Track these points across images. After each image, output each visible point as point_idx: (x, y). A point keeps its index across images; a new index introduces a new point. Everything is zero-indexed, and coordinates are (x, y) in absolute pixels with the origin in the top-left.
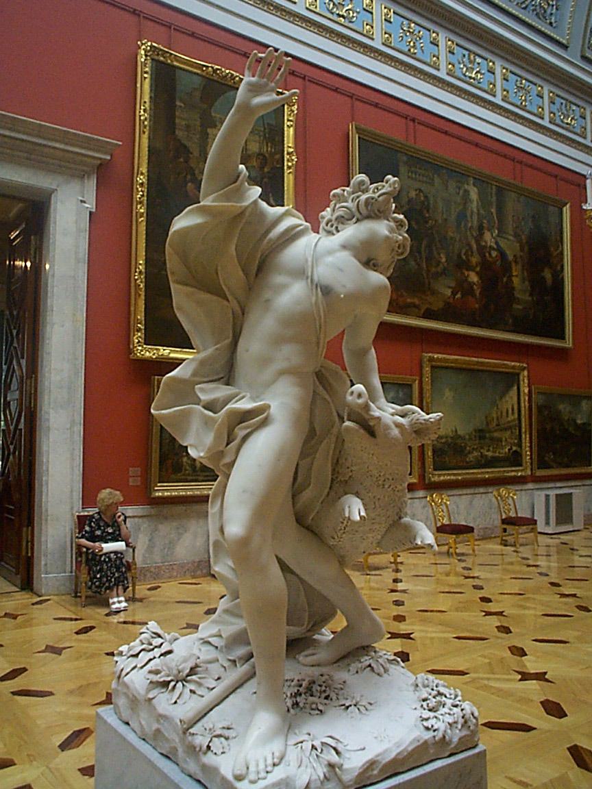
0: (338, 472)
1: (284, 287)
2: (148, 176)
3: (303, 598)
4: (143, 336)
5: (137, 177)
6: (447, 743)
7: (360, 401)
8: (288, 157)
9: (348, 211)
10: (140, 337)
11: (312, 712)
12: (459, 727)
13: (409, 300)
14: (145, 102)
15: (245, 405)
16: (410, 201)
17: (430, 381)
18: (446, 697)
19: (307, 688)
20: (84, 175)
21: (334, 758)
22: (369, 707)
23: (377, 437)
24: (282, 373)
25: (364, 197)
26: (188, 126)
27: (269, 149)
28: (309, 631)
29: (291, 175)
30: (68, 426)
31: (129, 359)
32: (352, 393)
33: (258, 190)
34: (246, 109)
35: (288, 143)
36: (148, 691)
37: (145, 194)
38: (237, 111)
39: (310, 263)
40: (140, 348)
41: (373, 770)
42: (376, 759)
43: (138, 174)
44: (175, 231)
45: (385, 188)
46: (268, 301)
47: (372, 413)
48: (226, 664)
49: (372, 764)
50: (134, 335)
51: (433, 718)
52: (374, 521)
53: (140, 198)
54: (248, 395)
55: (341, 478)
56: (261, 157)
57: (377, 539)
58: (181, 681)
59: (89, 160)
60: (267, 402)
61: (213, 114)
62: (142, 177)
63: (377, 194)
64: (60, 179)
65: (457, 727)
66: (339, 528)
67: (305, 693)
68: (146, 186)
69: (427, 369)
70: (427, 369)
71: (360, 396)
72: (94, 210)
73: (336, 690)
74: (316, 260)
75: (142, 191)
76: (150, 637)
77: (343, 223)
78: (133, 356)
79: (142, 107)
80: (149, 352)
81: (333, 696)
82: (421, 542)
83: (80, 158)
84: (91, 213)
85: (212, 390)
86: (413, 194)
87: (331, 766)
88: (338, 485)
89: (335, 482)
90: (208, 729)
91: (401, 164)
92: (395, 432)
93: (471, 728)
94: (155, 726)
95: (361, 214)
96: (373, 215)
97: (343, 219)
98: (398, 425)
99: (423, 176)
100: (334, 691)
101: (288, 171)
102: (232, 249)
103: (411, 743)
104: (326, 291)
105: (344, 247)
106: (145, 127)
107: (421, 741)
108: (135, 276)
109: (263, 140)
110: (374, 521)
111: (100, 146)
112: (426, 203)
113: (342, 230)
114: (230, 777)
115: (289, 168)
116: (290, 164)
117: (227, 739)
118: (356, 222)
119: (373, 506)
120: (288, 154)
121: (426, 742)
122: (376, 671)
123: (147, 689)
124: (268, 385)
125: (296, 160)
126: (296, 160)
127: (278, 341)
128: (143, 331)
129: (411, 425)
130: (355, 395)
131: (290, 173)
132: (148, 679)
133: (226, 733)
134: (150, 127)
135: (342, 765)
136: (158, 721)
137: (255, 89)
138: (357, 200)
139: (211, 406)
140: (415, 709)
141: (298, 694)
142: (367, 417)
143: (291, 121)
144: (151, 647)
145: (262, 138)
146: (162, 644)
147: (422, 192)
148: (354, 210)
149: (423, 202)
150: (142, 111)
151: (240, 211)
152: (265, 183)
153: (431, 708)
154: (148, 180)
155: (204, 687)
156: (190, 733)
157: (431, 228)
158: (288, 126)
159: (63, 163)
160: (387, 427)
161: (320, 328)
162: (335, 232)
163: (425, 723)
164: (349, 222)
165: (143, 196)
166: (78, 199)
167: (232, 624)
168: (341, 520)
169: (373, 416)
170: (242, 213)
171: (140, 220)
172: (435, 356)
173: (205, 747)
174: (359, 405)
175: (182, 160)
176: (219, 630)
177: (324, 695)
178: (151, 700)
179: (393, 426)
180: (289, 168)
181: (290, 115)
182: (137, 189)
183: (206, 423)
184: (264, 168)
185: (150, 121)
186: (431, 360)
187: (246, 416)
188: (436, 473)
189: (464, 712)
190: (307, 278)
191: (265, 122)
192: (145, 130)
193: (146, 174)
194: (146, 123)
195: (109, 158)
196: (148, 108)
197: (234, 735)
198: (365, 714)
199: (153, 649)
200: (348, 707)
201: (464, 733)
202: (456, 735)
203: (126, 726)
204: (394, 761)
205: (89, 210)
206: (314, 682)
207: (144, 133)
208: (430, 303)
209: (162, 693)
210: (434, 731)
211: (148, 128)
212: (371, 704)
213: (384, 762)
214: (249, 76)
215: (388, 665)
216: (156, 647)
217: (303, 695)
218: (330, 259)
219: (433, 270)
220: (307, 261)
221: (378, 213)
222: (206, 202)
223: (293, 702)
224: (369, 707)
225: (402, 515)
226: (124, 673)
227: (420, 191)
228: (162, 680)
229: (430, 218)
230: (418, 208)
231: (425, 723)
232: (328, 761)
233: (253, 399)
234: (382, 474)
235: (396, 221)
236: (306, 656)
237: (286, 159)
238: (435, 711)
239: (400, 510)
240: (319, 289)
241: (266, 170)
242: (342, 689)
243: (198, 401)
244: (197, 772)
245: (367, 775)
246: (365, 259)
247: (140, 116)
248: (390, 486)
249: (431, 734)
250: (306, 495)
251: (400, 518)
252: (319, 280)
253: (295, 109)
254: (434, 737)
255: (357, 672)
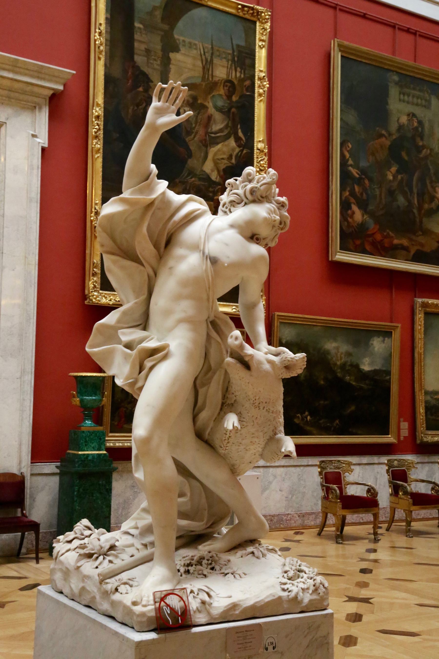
0: (227, 397)
1: (182, 258)
2: (105, 108)
3: (204, 500)
4: (99, 281)
5: (93, 109)
6: (299, 602)
7: (237, 343)
8: (259, 82)
9: (238, 196)
10: (96, 282)
11: (199, 576)
12: (310, 591)
13: (396, 242)
14: (100, 24)
15: (152, 344)
16: (401, 127)
17: (423, 329)
18: (305, 573)
19: (198, 562)
20: (35, 107)
21: (206, 598)
22: (243, 575)
23: (251, 369)
24: (180, 321)
25: (249, 186)
26: (148, 51)
27: (238, 75)
28: (208, 528)
29: (262, 103)
30: (18, 375)
31: (85, 304)
32: (232, 337)
33: (164, 184)
34: (154, 127)
35: (260, 66)
36: (78, 561)
37: (102, 127)
38: (147, 128)
39: (202, 241)
40: (96, 294)
41: (235, 610)
42: (238, 603)
43: (93, 106)
44: (102, 216)
45: (265, 179)
46: (171, 268)
47: (246, 351)
48: (140, 547)
49: (234, 606)
50: (89, 280)
51: (290, 584)
52: (253, 435)
53: (96, 133)
54: (156, 338)
55: (229, 402)
56: (229, 84)
57: (258, 451)
58: (103, 555)
59: (41, 91)
60: (167, 342)
61: (176, 36)
62: (97, 109)
63: (259, 184)
64: (9, 111)
65: (308, 592)
66: (224, 439)
67: (196, 565)
68: (103, 119)
69: (420, 317)
70: (420, 317)
71: (236, 338)
72: (46, 145)
73: (221, 565)
74: (208, 236)
75: (98, 125)
76: (82, 529)
77: (234, 206)
78: (89, 302)
79: (97, 30)
80: (106, 298)
81: (217, 567)
82: (285, 450)
83: (29, 88)
84: (43, 149)
85: (131, 333)
86: (404, 120)
87: (203, 603)
88: (226, 407)
89: (224, 405)
90: (117, 580)
91: (391, 85)
92: (267, 366)
93: (321, 594)
94: (81, 585)
95: (247, 199)
96: (257, 200)
97: (234, 203)
98: (270, 362)
99: (418, 98)
100: (219, 565)
101: (259, 99)
102: (144, 229)
103: (268, 597)
104: (214, 261)
105: (232, 226)
106: (101, 52)
107: (276, 597)
108: (91, 217)
109: (231, 65)
110: (253, 435)
111: (52, 77)
112: (420, 129)
113: (233, 212)
114: (129, 603)
115: (260, 95)
116: (261, 91)
117: (131, 586)
118: (244, 205)
119: (252, 424)
120: (260, 79)
121: (280, 598)
122: (256, 556)
123: (77, 560)
124: (170, 330)
125: (268, 86)
126: (268, 86)
127: (178, 298)
128: (100, 276)
129: (282, 362)
130: (234, 337)
131: (261, 101)
132: (78, 553)
133: (131, 582)
134: (106, 53)
135: (211, 604)
136: (83, 581)
137: (160, 112)
138: (245, 188)
139: (129, 346)
140: (278, 578)
141: (190, 565)
142: (243, 354)
143: (263, 41)
144: (83, 537)
145: (230, 62)
146: (91, 535)
147: (416, 117)
148: (242, 195)
149: (416, 128)
150: (97, 34)
151: (149, 202)
152: (233, 113)
153: (290, 577)
154: (104, 112)
155: (120, 559)
156: (105, 582)
157: (426, 157)
158: (260, 46)
159: (12, 94)
160: (260, 363)
161: (209, 288)
162: (228, 212)
163: (283, 586)
164: (239, 205)
165: (99, 129)
166: (29, 133)
167: (144, 519)
168: (225, 432)
169: (246, 353)
170: (152, 203)
171: (96, 156)
172: (430, 302)
173: (114, 589)
174: (237, 346)
175: (141, 89)
176: (136, 523)
177: (210, 567)
178: (78, 568)
179: (265, 362)
180: (260, 95)
181: (262, 34)
182: (93, 121)
183: (125, 358)
184: (231, 96)
185: (106, 45)
186: (424, 305)
187: (153, 352)
188: (430, 433)
189: (315, 581)
190: (200, 251)
191: (234, 42)
192: (101, 56)
193: (102, 105)
194: (102, 48)
195: (61, 88)
196: (104, 32)
197: (136, 585)
198: (239, 580)
199: (84, 539)
200: (227, 574)
201: (315, 597)
202: (307, 598)
203: (62, 595)
204: (253, 607)
205: (41, 145)
206: (204, 558)
207: (99, 59)
208: (422, 245)
209: (88, 562)
210: (289, 592)
211: (104, 53)
212: (245, 574)
213: (245, 606)
214: (156, 102)
215: (266, 552)
216: (87, 537)
217: (194, 566)
218: (219, 236)
219: (426, 206)
220: (200, 238)
221: (260, 198)
222: (126, 194)
223: (185, 569)
224: (243, 575)
225: (277, 432)
226: (60, 554)
227: (414, 115)
228: (87, 552)
229: (424, 147)
230: (409, 135)
231: (283, 586)
232: (201, 600)
233: (159, 340)
234: (257, 398)
235: (278, 202)
236: (205, 546)
237: (256, 85)
238: (293, 580)
239: (276, 428)
240: (208, 260)
241: (234, 98)
242: (226, 565)
243: (119, 342)
244: (108, 609)
245: (231, 613)
246: (250, 235)
247: (95, 41)
248: (264, 407)
249: (285, 594)
250: (203, 416)
251: (276, 434)
252: (209, 253)
253: (268, 27)
254: (288, 596)
255: (242, 557)
